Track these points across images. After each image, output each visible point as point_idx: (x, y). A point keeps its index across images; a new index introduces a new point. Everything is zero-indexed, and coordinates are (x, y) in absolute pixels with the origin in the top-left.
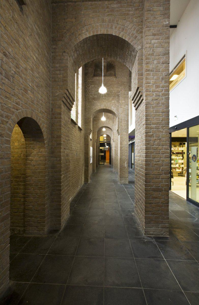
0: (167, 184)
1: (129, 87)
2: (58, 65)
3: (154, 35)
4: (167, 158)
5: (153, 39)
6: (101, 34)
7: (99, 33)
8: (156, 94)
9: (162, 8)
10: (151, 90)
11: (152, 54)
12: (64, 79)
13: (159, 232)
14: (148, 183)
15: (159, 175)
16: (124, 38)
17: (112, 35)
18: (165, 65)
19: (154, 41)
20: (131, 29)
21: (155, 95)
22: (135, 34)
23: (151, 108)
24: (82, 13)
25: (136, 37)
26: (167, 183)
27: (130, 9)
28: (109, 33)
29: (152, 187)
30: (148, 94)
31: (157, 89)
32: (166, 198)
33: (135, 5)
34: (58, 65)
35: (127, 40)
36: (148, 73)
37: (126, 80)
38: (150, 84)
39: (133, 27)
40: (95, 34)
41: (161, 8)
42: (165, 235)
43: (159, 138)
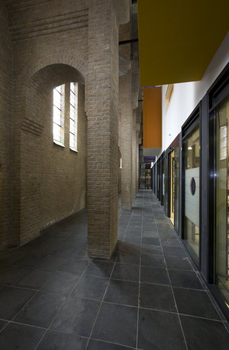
0: (108, 207)
1: (131, 103)
2: (17, 97)
3: (96, 61)
4: (108, 181)
5: (95, 65)
6: (53, 64)
7: (51, 63)
8: (98, 118)
9: (104, 34)
10: (93, 115)
11: (95, 80)
12: (22, 109)
13: (101, 254)
14: (90, 206)
15: (101, 198)
16: (73, 66)
17: (62, 64)
18: (106, 89)
19: (96, 67)
20: (79, 57)
21: (96, 119)
22: (83, 62)
23: (93, 132)
24: (37, 46)
25: (84, 64)
26: (107, 206)
27: (78, 37)
28: (60, 63)
29: (94, 210)
30: (91, 118)
31: (99, 113)
32: (107, 221)
33: (82, 34)
34: (17, 97)
35: (75, 67)
36: (91, 99)
37: (127, 96)
38: (93, 109)
39: (81, 54)
40: (48, 64)
41: (103, 35)
42: (106, 257)
43: (100, 161)
